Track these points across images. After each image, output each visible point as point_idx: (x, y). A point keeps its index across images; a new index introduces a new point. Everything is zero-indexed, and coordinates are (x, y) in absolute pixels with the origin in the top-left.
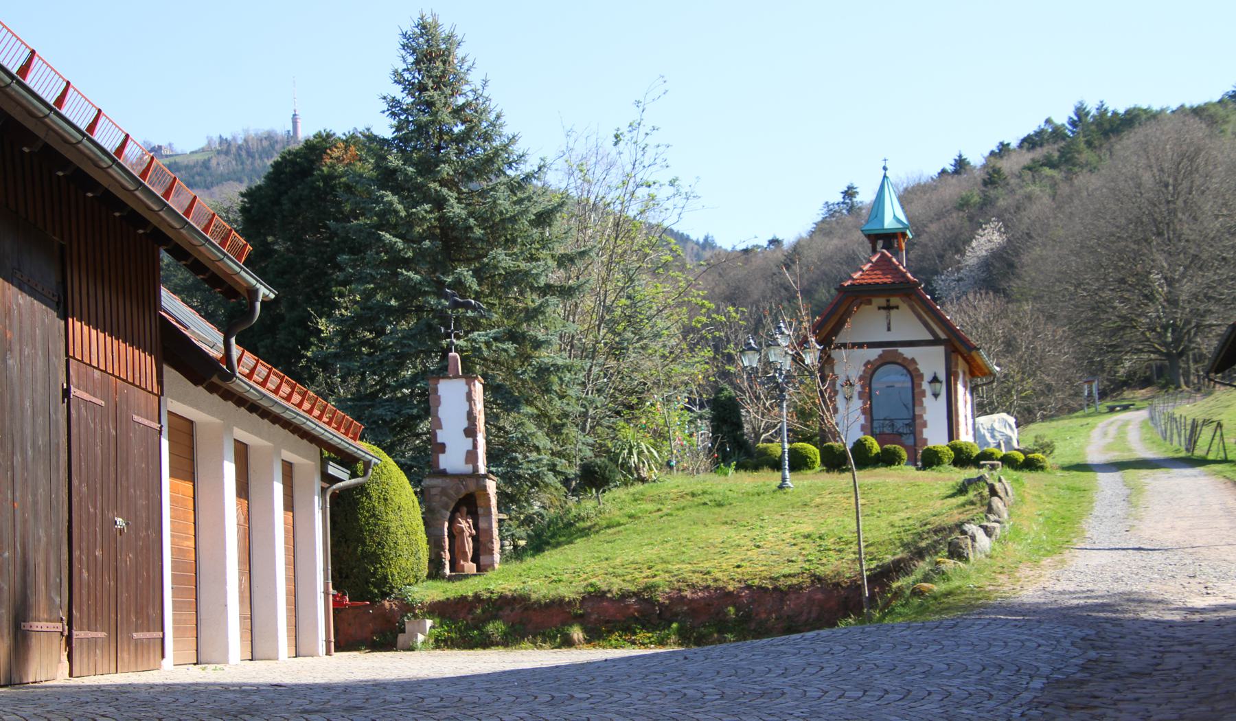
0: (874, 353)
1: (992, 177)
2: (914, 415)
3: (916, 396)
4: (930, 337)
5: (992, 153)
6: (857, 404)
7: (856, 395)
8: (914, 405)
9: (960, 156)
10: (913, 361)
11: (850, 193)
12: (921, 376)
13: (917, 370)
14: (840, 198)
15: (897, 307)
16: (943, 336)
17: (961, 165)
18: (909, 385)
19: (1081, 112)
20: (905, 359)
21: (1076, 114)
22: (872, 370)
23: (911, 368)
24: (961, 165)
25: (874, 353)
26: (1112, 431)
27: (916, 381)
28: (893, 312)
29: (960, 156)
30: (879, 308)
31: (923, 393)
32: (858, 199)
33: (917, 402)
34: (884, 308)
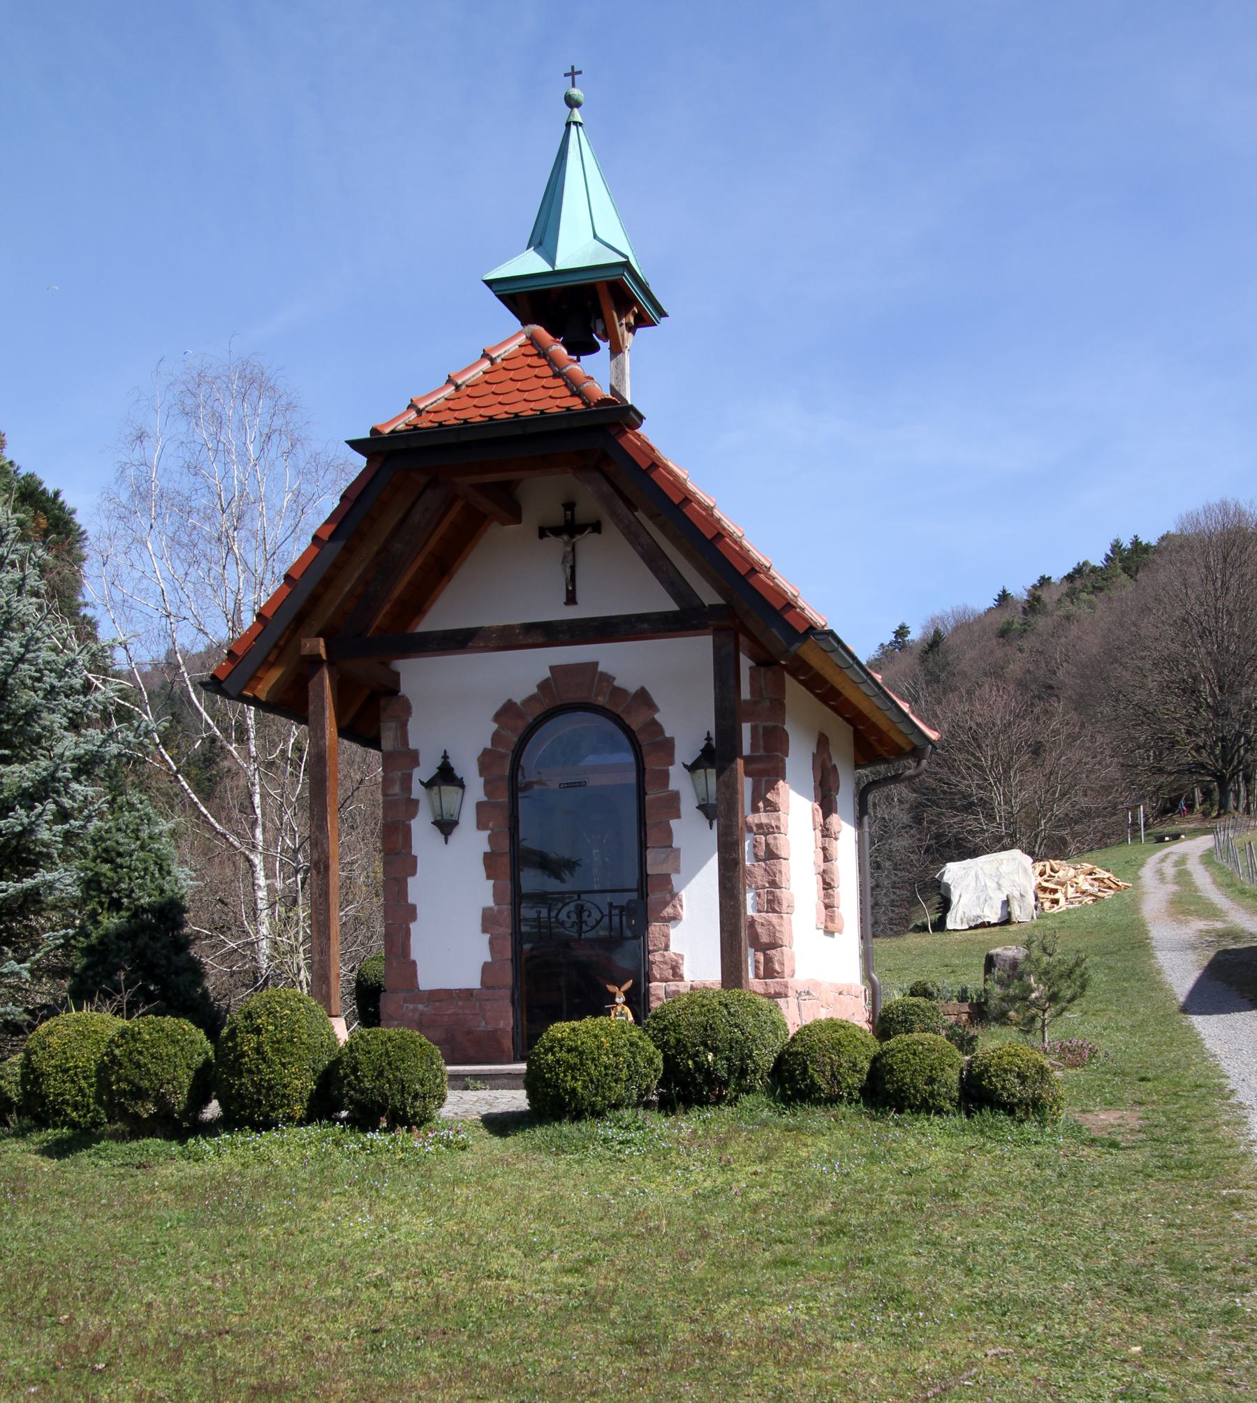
0: (524, 672)
1: (1034, 603)
2: (643, 876)
3: (647, 818)
4: (662, 602)
5: (1034, 587)
6: (473, 840)
7: (468, 818)
8: (643, 847)
9: (1004, 591)
10: (643, 697)
11: (902, 632)
12: (667, 747)
13: (656, 728)
14: (892, 637)
15: (597, 527)
16: (709, 596)
17: (1004, 597)
18: (631, 778)
19: (1116, 547)
20: (619, 692)
21: (1112, 552)
22: (521, 727)
23: (635, 723)
24: (1004, 597)
25: (524, 672)
26: (1170, 870)
27: (651, 764)
28: (586, 542)
29: (1004, 591)
30: (542, 533)
31: (672, 804)
32: (909, 637)
33: (653, 835)
34: (556, 531)
